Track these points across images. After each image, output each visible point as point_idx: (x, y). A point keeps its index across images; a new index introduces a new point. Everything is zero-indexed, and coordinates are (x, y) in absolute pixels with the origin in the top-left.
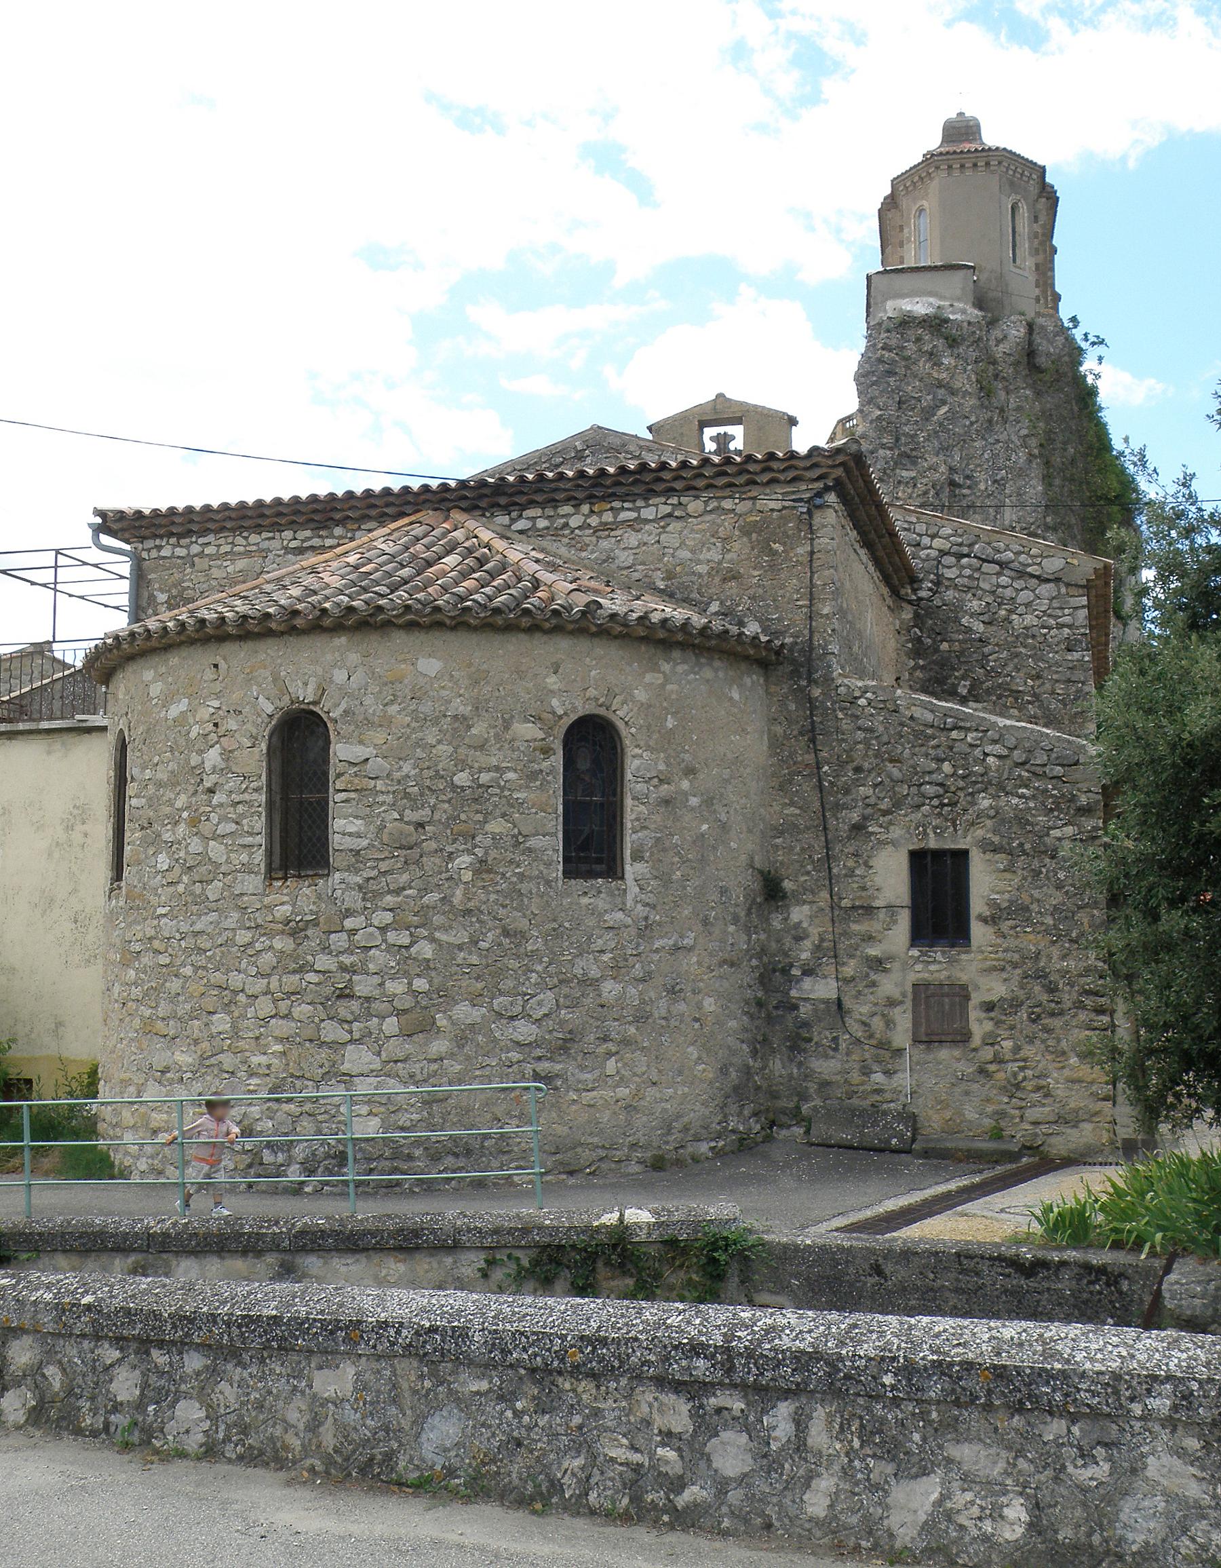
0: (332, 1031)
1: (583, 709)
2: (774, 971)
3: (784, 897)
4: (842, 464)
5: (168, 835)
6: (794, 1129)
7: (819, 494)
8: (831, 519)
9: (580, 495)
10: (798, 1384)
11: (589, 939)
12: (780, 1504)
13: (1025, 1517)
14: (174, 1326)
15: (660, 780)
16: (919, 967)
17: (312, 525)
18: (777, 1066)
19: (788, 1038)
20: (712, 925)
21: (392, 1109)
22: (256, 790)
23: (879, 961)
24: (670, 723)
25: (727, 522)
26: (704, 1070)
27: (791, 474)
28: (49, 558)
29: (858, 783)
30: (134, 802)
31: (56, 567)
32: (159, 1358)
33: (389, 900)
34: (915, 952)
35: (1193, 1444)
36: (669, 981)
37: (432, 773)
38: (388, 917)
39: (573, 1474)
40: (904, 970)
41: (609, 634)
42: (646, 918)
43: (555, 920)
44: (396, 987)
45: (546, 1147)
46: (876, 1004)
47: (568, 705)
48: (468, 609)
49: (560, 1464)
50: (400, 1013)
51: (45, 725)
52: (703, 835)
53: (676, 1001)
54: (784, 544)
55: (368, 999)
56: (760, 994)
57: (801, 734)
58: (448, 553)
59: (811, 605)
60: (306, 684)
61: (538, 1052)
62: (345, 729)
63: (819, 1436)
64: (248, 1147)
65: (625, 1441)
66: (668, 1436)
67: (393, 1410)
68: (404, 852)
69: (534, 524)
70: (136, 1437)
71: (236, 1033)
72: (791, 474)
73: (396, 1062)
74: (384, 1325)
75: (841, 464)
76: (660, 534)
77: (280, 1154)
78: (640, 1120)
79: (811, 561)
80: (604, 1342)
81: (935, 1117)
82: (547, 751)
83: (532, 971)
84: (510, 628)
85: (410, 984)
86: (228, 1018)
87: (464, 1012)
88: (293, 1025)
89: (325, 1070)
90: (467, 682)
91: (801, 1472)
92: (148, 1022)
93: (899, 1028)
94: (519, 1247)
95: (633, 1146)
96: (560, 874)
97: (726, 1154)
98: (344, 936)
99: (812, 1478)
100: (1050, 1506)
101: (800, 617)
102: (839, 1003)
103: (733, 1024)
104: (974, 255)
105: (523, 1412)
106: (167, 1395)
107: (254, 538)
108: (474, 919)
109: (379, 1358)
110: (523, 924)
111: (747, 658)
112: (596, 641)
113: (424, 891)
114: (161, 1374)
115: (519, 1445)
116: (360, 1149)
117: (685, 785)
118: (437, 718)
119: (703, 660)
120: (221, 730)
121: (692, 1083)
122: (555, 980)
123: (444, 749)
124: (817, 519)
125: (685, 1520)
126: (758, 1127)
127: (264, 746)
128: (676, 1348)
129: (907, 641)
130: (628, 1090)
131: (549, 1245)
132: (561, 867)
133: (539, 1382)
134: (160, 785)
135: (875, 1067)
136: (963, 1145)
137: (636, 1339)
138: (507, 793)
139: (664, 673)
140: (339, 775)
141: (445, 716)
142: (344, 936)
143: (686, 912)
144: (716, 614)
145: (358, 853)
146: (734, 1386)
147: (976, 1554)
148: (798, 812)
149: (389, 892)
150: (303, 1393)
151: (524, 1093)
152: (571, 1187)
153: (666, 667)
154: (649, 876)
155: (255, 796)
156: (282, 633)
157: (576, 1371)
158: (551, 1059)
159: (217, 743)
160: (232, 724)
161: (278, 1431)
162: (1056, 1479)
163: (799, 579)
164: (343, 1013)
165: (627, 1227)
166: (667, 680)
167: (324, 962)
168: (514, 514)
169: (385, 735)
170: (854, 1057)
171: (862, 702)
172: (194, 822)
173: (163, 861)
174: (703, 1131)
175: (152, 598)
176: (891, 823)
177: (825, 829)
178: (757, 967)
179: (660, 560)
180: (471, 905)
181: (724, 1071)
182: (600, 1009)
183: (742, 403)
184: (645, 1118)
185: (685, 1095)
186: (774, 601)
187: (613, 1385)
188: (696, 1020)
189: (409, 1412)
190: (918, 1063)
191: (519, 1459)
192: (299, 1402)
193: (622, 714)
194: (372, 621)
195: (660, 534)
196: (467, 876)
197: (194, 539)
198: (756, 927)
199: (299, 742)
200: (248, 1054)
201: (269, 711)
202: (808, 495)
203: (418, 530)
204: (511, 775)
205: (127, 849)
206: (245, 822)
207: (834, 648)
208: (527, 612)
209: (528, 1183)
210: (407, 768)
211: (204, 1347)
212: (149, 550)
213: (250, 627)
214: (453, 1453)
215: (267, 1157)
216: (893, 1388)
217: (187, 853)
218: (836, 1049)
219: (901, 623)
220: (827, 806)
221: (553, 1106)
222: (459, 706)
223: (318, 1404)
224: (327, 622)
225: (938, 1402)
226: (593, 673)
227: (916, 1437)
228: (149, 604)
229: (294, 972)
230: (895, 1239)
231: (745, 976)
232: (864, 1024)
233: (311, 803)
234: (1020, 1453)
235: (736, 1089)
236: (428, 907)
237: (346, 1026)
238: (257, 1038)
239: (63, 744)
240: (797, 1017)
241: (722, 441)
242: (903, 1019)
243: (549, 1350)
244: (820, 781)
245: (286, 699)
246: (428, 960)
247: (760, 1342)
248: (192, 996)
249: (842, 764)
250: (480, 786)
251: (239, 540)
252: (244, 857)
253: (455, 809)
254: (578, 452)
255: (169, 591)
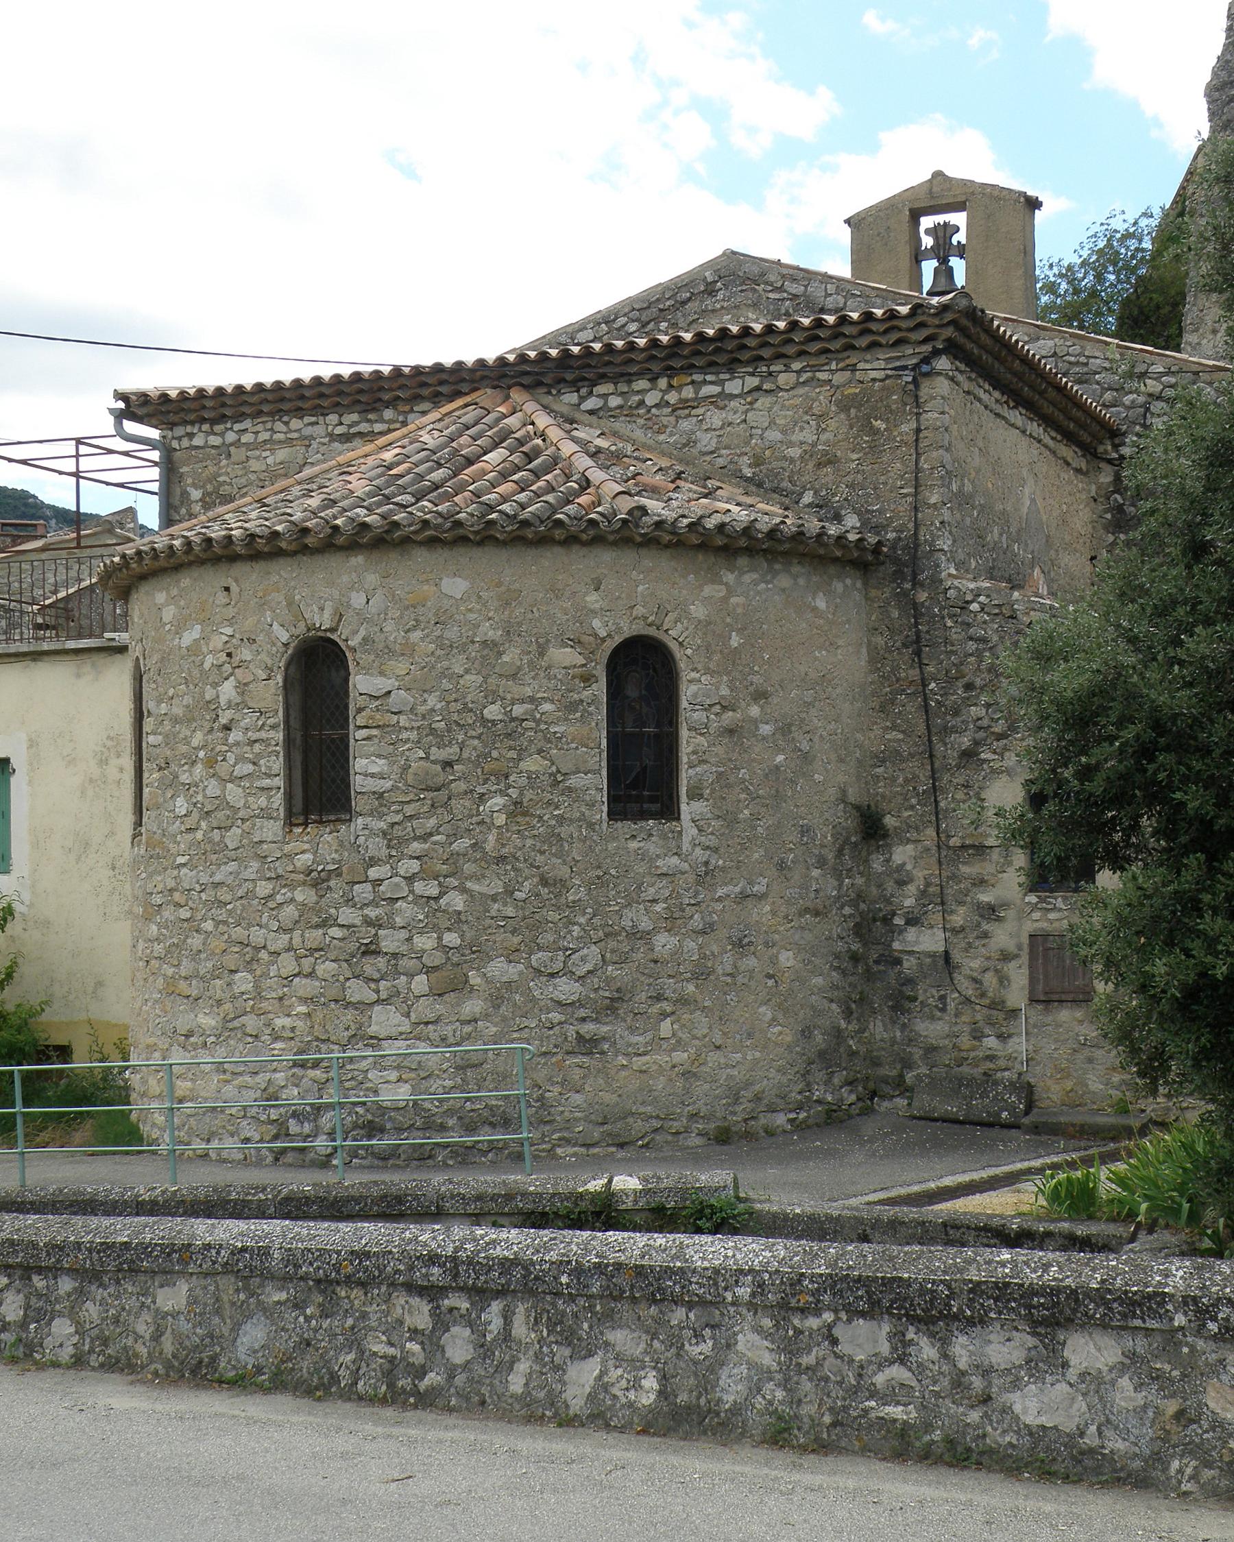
0: (358, 991)
1: (638, 629)
2: (875, 920)
3: (885, 836)
4: (953, 322)
5: (185, 776)
6: (898, 1100)
7: (926, 360)
8: (946, 389)
9: (656, 367)
10: (503, 1286)
11: (639, 887)
12: (491, 1385)
13: (656, 1386)
14: (48, 1254)
15: (724, 708)
16: (1036, 915)
17: (358, 408)
18: (878, 1029)
19: (889, 997)
20: (790, 869)
21: (423, 1074)
22: (273, 727)
23: (992, 909)
24: (735, 641)
25: (823, 394)
26: (781, 1033)
27: (894, 337)
28: (70, 448)
29: (968, 702)
30: (151, 739)
31: (77, 456)
32: (39, 1282)
33: (416, 847)
34: (1032, 898)
35: (767, 1323)
36: (735, 933)
37: (459, 706)
38: (415, 866)
39: (347, 1367)
40: (1020, 919)
41: (659, 543)
42: (707, 863)
43: (599, 867)
44: (424, 942)
45: (593, 1117)
46: (988, 958)
47: (612, 626)
48: (491, 523)
49: (337, 1359)
50: (429, 970)
51: (71, 644)
52: (777, 767)
53: (743, 955)
54: (887, 421)
55: (395, 955)
56: (855, 947)
57: (905, 645)
58: (496, 445)
59: (916, 494)
60: (322, 609)
61: (582, 1013)
62: (364, 658)
63: (520, 1329)
64: (273, 1117)
65: (384, 1338)
66: (415, 1333)
67: (217, 1320)
68: (432, 794)
69: (606, 402)
70: (20, 1352)
71: (259, 995)
72: (894, 337)
73: (427, 1023)
74: (208, 1247)
75: (949, 323)
76: (746, 412)
77: (306, 1124)
78: (701, 1088)
79: (917, 440)
80: (367, 1255)
81: (1055, 1088)
82: (587, 679)
83: (575, 924)
84: (543, 541)
85: (440, 938)
86: (250, 977)
87: (499, 969)
88: (317, 984)
89: (351, 1032)
90: (496, 604)
91: (507, 1358)
92: (171, 982)
93: (1014, 986)
94: (503, 1214)
95: (694, 1116)
96: (605, 815)
97: (809, 1127)
98: (368, 887)
99: (513, 1362)
100: (673, 1377)
101: (904, 506)
102: (947, 956)
103: (818, 981)
104: (848, 221)
105: (312, 1317)
106: (45, 1315)
107: (295, 424)
108: (509, 867)
109: (207, 1275)
110: (564, 872)
111: (836, 560)
112: (643, 551)
113: (454, 836)
114: (40, 1296)
115: (308, 1344)
116: (390, 1117)
117: (755, 711)
118: (465, 644)
119: (777, 566)
120: (236, 660)
121: (765, 1047)
122: (601, 933)
123: (472, 679)
124: (924, 392)
125: (426, 1400)
126: (853, 1098)
127: (280, 679)
128: (418, 1258)
129: (1106, 511)
130: (686, 1054)
131: (533, 1212)
132: (605, 808)
133: (323, 1292)
134: (176, 721)
135: (987, 1031)
136: (1078, 1119)
137: (390, 1252)
138: (543, 727)
139: (726, 584)
140: (360, 710)
141: (473, 642)
142: (368, 887)
143: (756, 855)
144: (809, 505)
145: (381, 795)
146: (461, 1289)
147: (623, 1417)
148: (901, 736)
149: (416, 838)
150: (149, 1308)
151: (566, 1057)
152: (623, 1160)
153: (730, 577)
154: (709, 815)
155: (272, 734)
156: (295, 553)
157: (349, 1281)
158: (597, 1020)
159: (231, 674)
160: (246, 654)
161: (130, 1342)
162: (678, 1355)
163: (903, 463)
164: (369, 970)
165: (613, 1194)
166: (730, 592)
167: (348, 915)
168: (584, 391)
169: (408, 665)
170: (964, 1018)
171: (975, 607)
172: (211, 763)
173: (181, 806)
174: (779, 1101)
175: (185, 495)
176: (1005, 749)
177: (931, 756)
178: (851, 915)
179: (747, 443)
180: (505, 851)
181: (806, 1033)
182: (652, 965)
183: (965, 183)
184: (707, 1086)
185: (756, 1061)
186: (875, 489)
187: (376, 1291)
188: (770, 976)
189: (228, 1321)
190: (1035, 1026)
191: (308, 1357)
192: (146, 1316)
193: (680, 637)
194: (388, 538)
195: (746, 412)
196: (501, 819)
197: (229, 425)
198: (849, 870)
199: (317, 672)
200: (271, 1016)
201: (284, 640)
202: (914, 361)
203: (471, 415)
204: (547, 707)
205: (146, 791)
206: (262, 762)
207: (945, 543)
208: (559, 523)
209: (572, 1156)
210: (432, 701)
211: (72, 1272)
212: (179, 439)
213: (259, 547)
214: (260, 1354)
215: (293, 1126)
216: (568, 1286)
217: (205, 796)
218: (943, 1010)
219: (1099, 488)
220: (934, 730)
221: (599, 1071)
222: (489, 632)
223: (160, 1315)
224: (340, 540)
225: (602, 1297)
226: (640, 588)
227: (585, 1326)
228: (182, 502)
229: (317, 926)
230: (936, 1214)
231: (835, 925)
232: (975, 980)
233: (333, 741)
234: (654, 1336)
235: (822, 1054)
236: (458, 854)
237: (373, 986)
238: (281, 999)
239: (93, 665)
240: (900, 973)
241: (941, 234)
242: (1019, 975)
243: (328, 1263)
244: (925, 700)
245: (302, 625)
246: (459, 913)
247: (479, 1252)
248: (213, 954)
249: (951, 680)
250: (513, 720)
251: (279, 426)
252: (263, 802)
253: (485, 746)
254: (708, 284)
255: (203, 487)
